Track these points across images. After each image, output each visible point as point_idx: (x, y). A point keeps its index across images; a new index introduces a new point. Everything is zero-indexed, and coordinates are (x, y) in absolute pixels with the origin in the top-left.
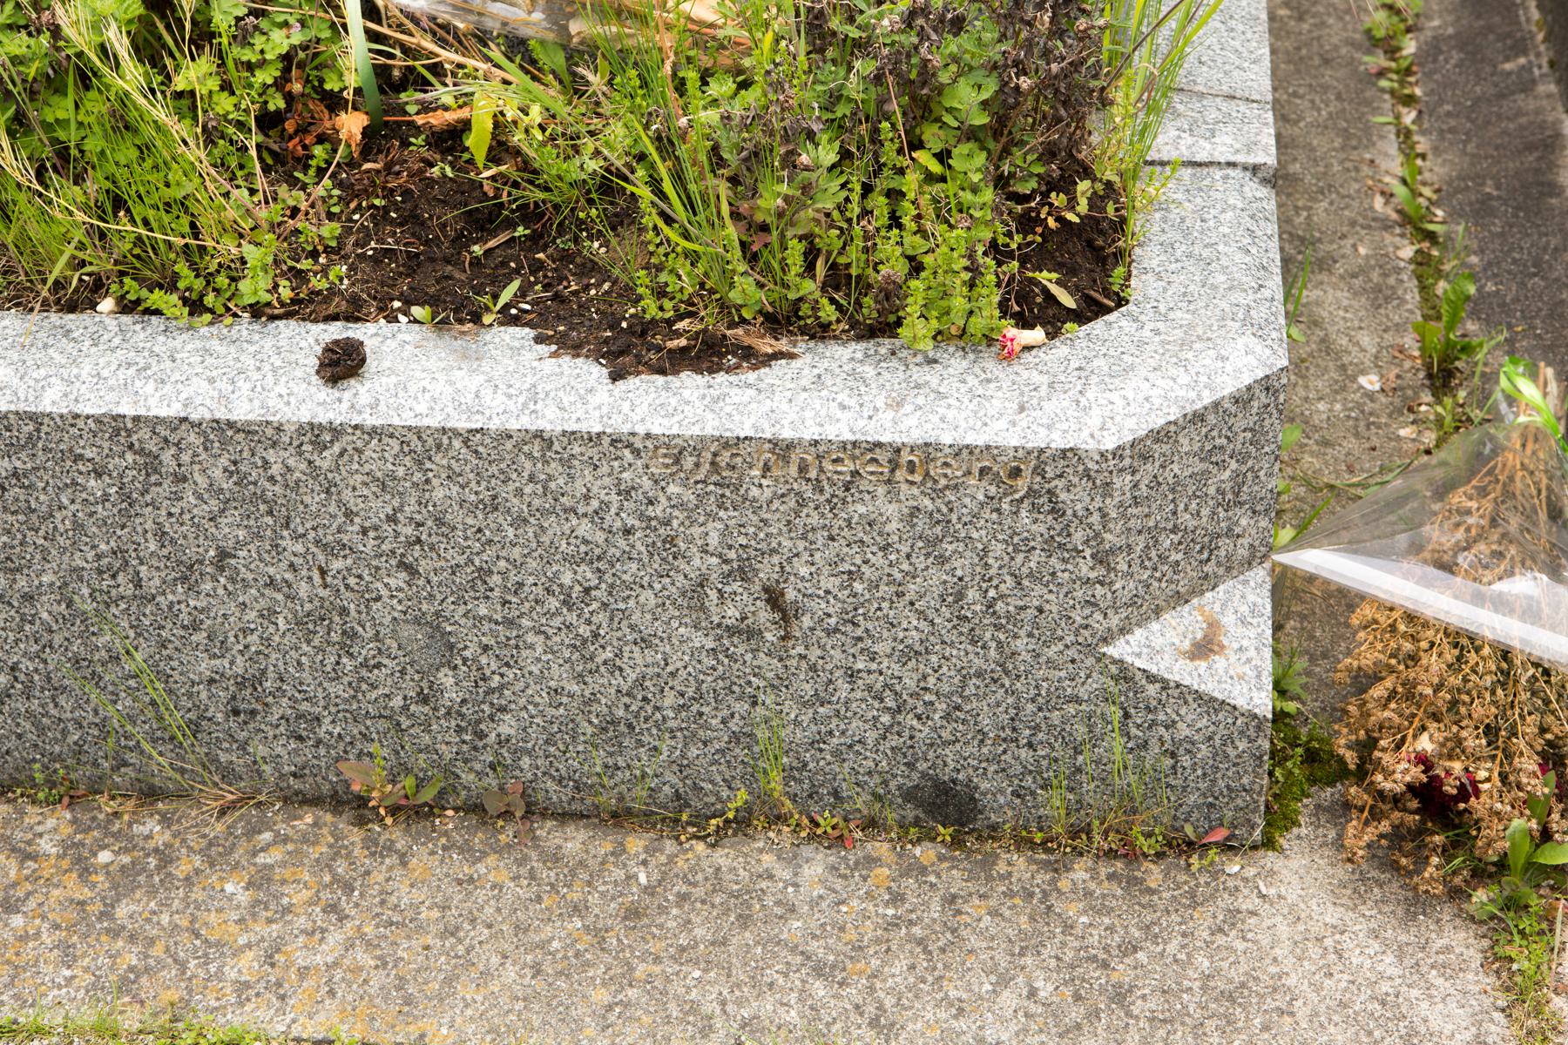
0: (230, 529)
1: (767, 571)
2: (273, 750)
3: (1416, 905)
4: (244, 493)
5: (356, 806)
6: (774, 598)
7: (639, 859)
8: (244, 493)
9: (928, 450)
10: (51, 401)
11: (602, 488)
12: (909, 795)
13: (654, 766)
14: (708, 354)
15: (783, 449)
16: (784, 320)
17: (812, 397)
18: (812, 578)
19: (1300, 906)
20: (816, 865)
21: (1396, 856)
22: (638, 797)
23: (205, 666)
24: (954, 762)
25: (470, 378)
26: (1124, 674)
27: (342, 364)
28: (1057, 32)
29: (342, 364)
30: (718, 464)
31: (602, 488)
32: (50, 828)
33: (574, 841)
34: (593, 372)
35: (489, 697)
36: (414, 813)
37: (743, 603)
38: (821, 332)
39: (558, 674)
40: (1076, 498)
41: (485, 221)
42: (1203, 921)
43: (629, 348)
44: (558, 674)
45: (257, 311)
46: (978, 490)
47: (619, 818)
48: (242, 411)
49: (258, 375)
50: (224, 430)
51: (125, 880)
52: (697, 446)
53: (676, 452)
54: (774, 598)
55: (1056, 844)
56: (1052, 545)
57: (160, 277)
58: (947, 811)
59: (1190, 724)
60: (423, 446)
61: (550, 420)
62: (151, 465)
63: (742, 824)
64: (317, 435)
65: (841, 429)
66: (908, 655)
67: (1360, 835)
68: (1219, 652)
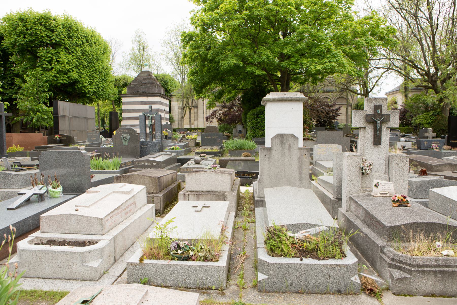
0: (293, 271)
1: (329, 274)
2: (293, 289)
3: (372, 297)
4: (295, 269)
5: (299, 293)
6: (329, 276)
7: (319, 296)
8: (295, 269)
9: (340, 265)
10: (283, 262)
11: (319, 268)
12: (337, 291)
13: (319, 289)
14: (324, 259)
15: (331, 265)
16: (328, 257)
17: (331, 262)
18: (332, 274)
19: (364, 297)
20: (332, 296)
21: (369, 295)
22: (318, 292)
23: (289, 282)
24: (340, 288)
25: (308, 261)
26: (351, 281)
27: (301, 260)
28: (44, 56)
29: (301, 260)
30: (326, 266)
31: (319, 268)
32: (277, 295)
33: (314, 295)
34: (317, 260)
35: (309, 284)
36: (303, 293)
37: (327, 276)
38: (330, 258)
39: (314, 282)
40: (349, 268)
41: (305, 252)
42: (359, 298)
43: (319, 259)
44: (314, 282)
45: (293, 257)
46: (343, 267)
47: (317, 293)
48: (296, 263)
49: (297, 261)
50: (295, 264)
51: (285, 297)
52: (325, 265)
53: (324, 265)
54: (329, 276)
55: (348, 294)
56: (347, 271)
57: (285, 255)
58: (339, 292)
59: (356, 284)
60: (307, 265)
61: (316, 263)
62: (289, 267)
63: (325, 294)
64: (301, 264)
65: (334, 263)
66: (338, 280)
67: (367, 292)
68: (356, 279)
